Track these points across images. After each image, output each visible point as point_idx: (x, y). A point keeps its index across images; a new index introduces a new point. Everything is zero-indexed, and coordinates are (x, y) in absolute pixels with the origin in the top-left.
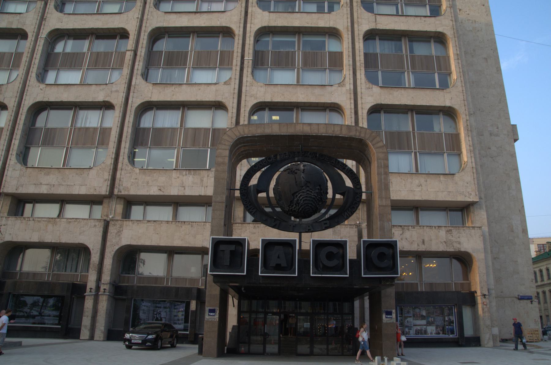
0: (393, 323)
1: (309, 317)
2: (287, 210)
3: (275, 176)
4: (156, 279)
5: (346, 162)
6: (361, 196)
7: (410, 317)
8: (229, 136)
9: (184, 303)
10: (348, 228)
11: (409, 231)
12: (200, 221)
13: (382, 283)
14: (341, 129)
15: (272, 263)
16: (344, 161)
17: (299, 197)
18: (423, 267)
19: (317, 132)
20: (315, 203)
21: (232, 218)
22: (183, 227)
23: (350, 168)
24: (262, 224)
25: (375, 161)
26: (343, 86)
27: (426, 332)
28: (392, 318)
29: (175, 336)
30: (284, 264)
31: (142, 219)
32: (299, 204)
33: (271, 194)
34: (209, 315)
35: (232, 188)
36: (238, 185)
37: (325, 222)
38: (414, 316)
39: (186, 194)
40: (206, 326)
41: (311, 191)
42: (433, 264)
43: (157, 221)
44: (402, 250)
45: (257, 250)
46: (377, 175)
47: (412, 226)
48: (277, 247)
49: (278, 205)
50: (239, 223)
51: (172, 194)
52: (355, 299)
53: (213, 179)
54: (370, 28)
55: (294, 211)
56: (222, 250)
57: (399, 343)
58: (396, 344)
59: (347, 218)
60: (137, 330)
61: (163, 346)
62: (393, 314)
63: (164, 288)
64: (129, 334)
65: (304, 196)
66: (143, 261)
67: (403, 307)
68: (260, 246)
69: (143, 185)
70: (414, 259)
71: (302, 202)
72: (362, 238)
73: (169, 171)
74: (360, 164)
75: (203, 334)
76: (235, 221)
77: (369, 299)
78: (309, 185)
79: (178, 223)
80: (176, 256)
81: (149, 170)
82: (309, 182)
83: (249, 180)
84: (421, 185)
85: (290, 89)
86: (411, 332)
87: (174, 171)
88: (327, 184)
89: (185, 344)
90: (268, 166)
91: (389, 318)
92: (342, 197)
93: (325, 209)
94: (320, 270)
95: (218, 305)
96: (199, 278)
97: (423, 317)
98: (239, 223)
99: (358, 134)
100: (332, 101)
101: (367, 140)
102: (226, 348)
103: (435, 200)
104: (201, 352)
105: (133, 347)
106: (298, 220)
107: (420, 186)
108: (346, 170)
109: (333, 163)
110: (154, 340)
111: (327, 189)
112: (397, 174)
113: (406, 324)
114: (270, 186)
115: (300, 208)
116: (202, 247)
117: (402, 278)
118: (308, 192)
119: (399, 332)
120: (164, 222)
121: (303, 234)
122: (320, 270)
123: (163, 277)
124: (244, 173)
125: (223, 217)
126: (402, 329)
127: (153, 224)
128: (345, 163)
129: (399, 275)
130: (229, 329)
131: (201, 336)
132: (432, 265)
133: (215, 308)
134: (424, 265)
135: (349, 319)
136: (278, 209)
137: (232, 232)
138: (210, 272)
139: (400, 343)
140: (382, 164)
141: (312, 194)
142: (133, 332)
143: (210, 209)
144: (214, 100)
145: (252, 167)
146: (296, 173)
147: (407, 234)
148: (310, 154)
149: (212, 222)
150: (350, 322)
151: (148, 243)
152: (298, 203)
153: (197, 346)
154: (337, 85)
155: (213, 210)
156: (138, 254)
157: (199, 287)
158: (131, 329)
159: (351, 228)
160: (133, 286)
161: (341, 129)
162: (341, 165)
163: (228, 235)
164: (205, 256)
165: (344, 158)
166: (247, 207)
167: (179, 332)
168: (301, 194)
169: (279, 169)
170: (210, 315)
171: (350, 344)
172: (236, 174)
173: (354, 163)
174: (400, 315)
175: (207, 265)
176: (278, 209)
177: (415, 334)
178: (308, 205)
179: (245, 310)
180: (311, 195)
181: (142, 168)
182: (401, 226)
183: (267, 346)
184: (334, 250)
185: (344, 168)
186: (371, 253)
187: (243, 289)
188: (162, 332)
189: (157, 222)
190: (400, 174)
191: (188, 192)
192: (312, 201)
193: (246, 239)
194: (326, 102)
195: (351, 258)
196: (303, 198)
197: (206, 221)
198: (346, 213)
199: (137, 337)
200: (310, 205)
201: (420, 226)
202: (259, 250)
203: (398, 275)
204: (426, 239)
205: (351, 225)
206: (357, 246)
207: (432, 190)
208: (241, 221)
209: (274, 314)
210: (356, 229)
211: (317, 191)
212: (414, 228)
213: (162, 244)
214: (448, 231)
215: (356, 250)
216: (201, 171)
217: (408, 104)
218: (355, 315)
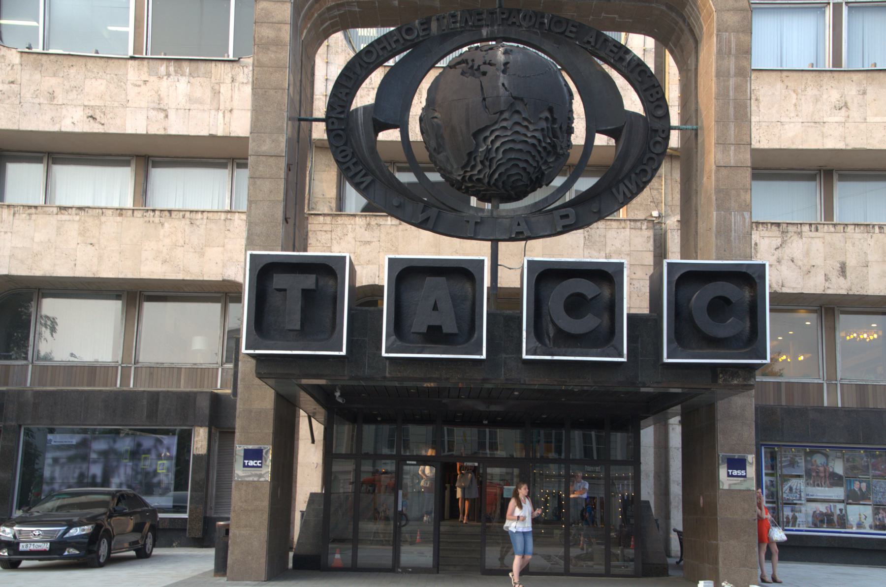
0: (749, 490)
1: (516, 471)
2: (459, 178)
3: (424, 81)
4: (92, 371)
5: (627, 39)
6: (667, 138)
7: (799, 476)
9: (174, 434)
10: (628, 230)
11: (801, 237)
12: (215, 209)
13: (720, 381)
15: (419, 324)
16: (622, 37)
17: (493, 142)
18: (838, 341)
20: (538, 158)
21: (306, 201)
22: (166, 225)
23: (639, 59)
24: (389, 218)
25: (711, 36)
27: (843, 521)
28: (745, 477)
29: (147, 526)
30: (450, 327)
31: (42, 203)
32: (491, 160)
33: (415, 134)
34: (244, 466)
35: (303, 116)
36: (320, 108)
37: (563, 212)
38: (808, 473)
39: (172, 131)
40: (237, 496)
41: (525, 123)
42: (869, 330)
43: (89, 208)
44: (779, 290)
45: (376, 290)
46: (714, 79)
47: (810, 225)
48: (430, 281)
49: (433, 165)
50: (325, 215)
51: (129, 131)
52: (642, 423)
53: (248, 89)
55: (479, 180)
56: (278, 287)
57: (764, 547)
58: (757, 549)
59: (626, 201)
60: (36, 514)
61: (112, 555)
62: (748, 468)
63: (117, 394)
64: (11, 526)
65: (506, 139)
66: (49, 323)
67: (776, 449)
68: (383, 279)
69: (37, 101)
70: (814, 316)
71: (500, 156)
72: (665, 258)
73: (116, 61)
74: (666, 45)
75: (228, 519)
76: (313, 209)
77: (683, 423)
78: (519, 107)
79: (152, 214)
80: (149, 308)
81: (52, 57)
82: (522, 100)
83: (352, 94)
84: (846, 105)
86: (801, 517)
87: (131, 62)
88: (571, 104)
89: (177, 546)
90: (405, 53)
91: (737, 476)
92: (612, 142)
93: (565, 175)
94: (547, 341)
95: (270, 438)
96: (215, 366)
97: (835, 480)
98: (325, 215)
102: (291, 554)
104: (221, 567)
105: (24, 563)
106: (488, 206)
107: (844, 109)
108: (625, 64)
109: (589, 42)
110: (87, 540)
111: (570, 119)
112: (774, 74)
113: (785, 496)
114: (412, 109)
116: (224, 281)
117: (776, 368)
118: (518, 128)
119: (764, 516)
120: (110, 212)
121: (502, 245)
122: (547, 341)
123: (113, 364)
124: (335, 71)
125: (281, 196)
126: (773, 508)
127: (77, 218)
128: (623, 42)
129: (768, 361)
130: (301, 503)
131: (222, 523)
132: (865, 336)
133: (262, 447)
134: (843, 334)
135: (627, 478)
136: (435, 177)
137: (305, 238)
138: (246, 349)
139: (768, 547)
140: (733, 45)
142: (22, 522)
143: (243, 175)
145: (359, 56)
146: (484, 74)
147: (796, 247)
148: (524, 17)
149: (249, 213)
150: (628, 485)
151: (63, 271)
152: (488, 159)
153: (212, 552)
155: (251, 178)
156: (33, 303)
157: (216, 391)
158: (17, 513)
159: (635, 229)
160: (20, 393)
162: (611, 51)
163: (294, 246)
164: (232, 306)
165: (620, 29)
166: (348, 168)
167: (161, 515)
168: (497, 133)
169: (437, 63)
170: (248, 466)
171: (627, 546)
172: (313, 74)
173: (650, 42)
174: (770, 472)
175: (238, 331)
176: (435, 177)
177: (811, 525)
178: (517, 165)
179: (343, 450)
180: (525, 135)
181: (29, 48)
182: (778, 225)
183: (404, 548)
184: (587, 288)
185: (622, 59)
186: (691, 299)
187: (338, 394)
188: (110, 517)
189: (90, 211)
190: (785, 74)
191: (177, 126)
193: (345, 257)
195: (633, 311)
196: (503, 144)
197: (233, 209)
198: (622, 187)
199: (37, 533)
200: (522, 165)
201: (835, 225)
202: (383, 287)
203: (765, 358)
204: (851, 262)
205: (635, 221)
206: (651, 277)
207: (878, 119)
208: (332, 209)
209: (424, 461)
210: (650, 233)
211: (543, 124)
212: (817, 230)
213: (108, 271)
215: (647, 290)
216: (213, 64)
218: (643, 467)
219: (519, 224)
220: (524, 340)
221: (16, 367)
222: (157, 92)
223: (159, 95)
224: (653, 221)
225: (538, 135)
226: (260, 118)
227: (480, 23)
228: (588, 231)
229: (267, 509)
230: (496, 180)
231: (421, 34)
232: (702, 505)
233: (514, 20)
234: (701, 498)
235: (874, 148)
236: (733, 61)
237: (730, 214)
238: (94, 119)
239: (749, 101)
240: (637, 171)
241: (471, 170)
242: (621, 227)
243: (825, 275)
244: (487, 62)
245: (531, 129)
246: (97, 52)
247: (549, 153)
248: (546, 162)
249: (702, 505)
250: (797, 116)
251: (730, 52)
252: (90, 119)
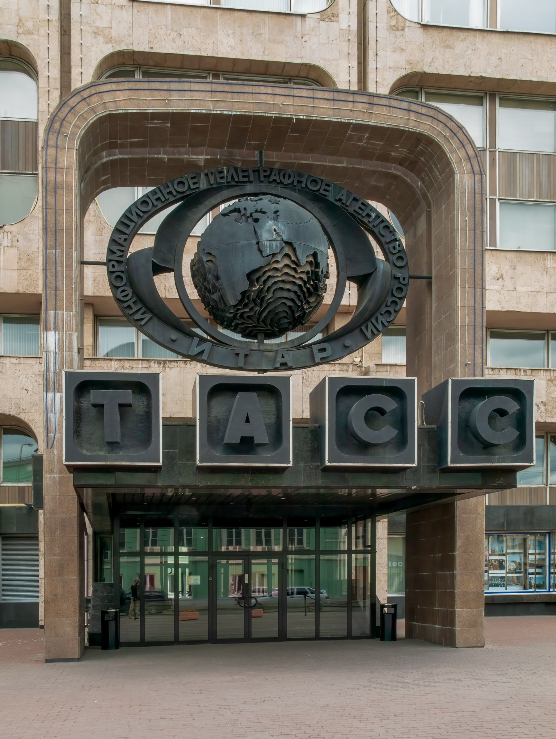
20: (302, 297)
26: (335, 19)
37: (322, 346)
55: (249, 317)
79: (400, 70)
83: (129, 240)
100: (304, 61)
103: (529, 311)
107: (500, 279)
115: (264, 310)
118: (286, 270)
146: (256, 220)
154: (318, 16)
192: (295, 292)
194: (289, 61)
200: (289, 303)
214: (550, 380)
217: (488, 76)
220: (108, 463)
221: (541, 156)
224: (357, 364)
225: (304, 276)
228: (305, 373)
230: (265, 317)
235: (522, 311)
240: (383, 312)
242: (332, 369)
244: (259, 210)
245: (299, 271)
247: (310, 294)
248: (308, 302)
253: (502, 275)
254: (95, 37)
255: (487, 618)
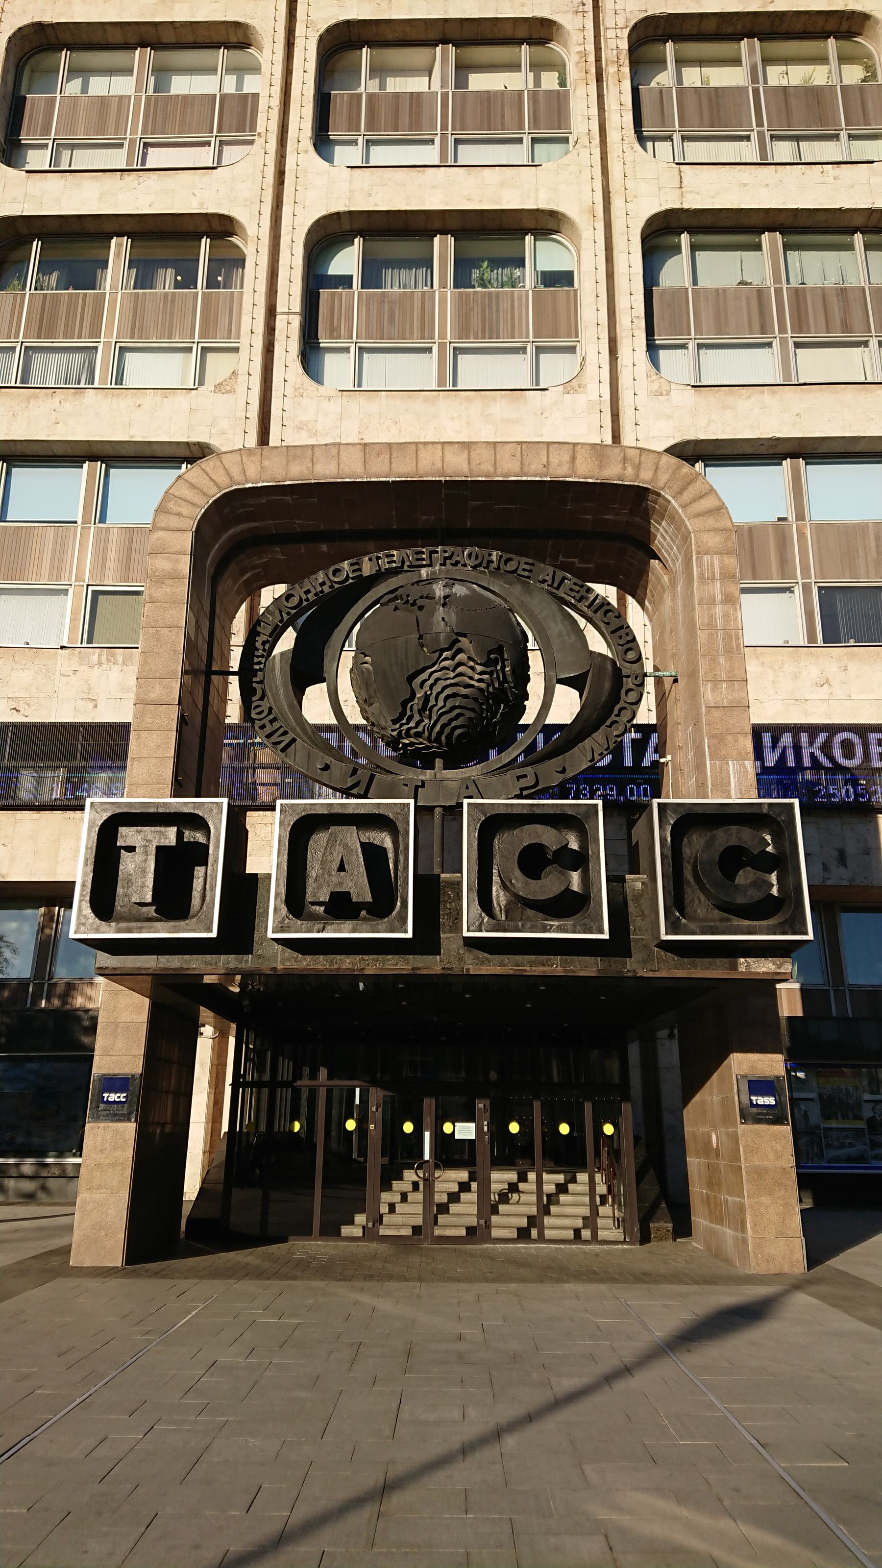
8: (193, 486)
14: (573, 458)
19: (491, 469)
41: (471, 664)
54: (663, 208)
71: (441, 703)
84: (827, 681)
85: (418, 403)
99: (630, 471)
101: (662, 489)
107: (826, 686)
109: (544, 581)
141: (477, 677)
144: (184, 439)
146: (421, 608)
154: (561, 388)
161: (573, 458)
168: (437, 675)
204: (851, 849)
219: (467, 788)
222: (87, 682)
223: (89, 685)
226: (149, 660)
227: (419, 563)
229: (129, 1163)
231: (351, 575)
232: (715, 1145)
233: (458, 559)
234: (714, 1136)
236: (718, 585)
237: (727, 764)
238: (18, 711)
239: (741, 631)
241: (408, 723)
243: (823, 864)
246: (28, 644)
249: (715, 1145)
250: (776, 693)
251: (713, 578)
252: (14, 711)
253: (827, 680)
254: (298, 432)
255: (61, 876)
